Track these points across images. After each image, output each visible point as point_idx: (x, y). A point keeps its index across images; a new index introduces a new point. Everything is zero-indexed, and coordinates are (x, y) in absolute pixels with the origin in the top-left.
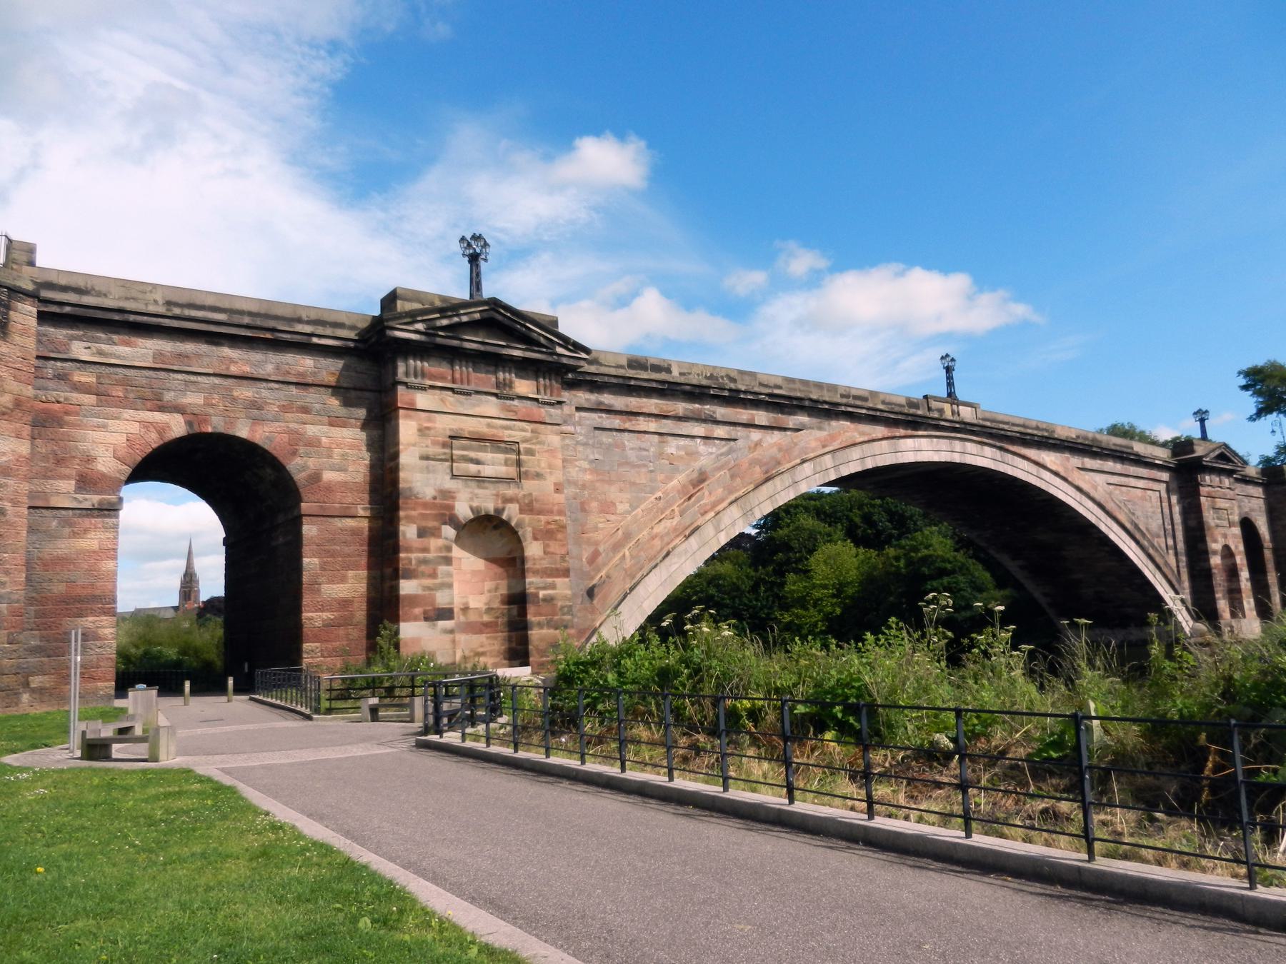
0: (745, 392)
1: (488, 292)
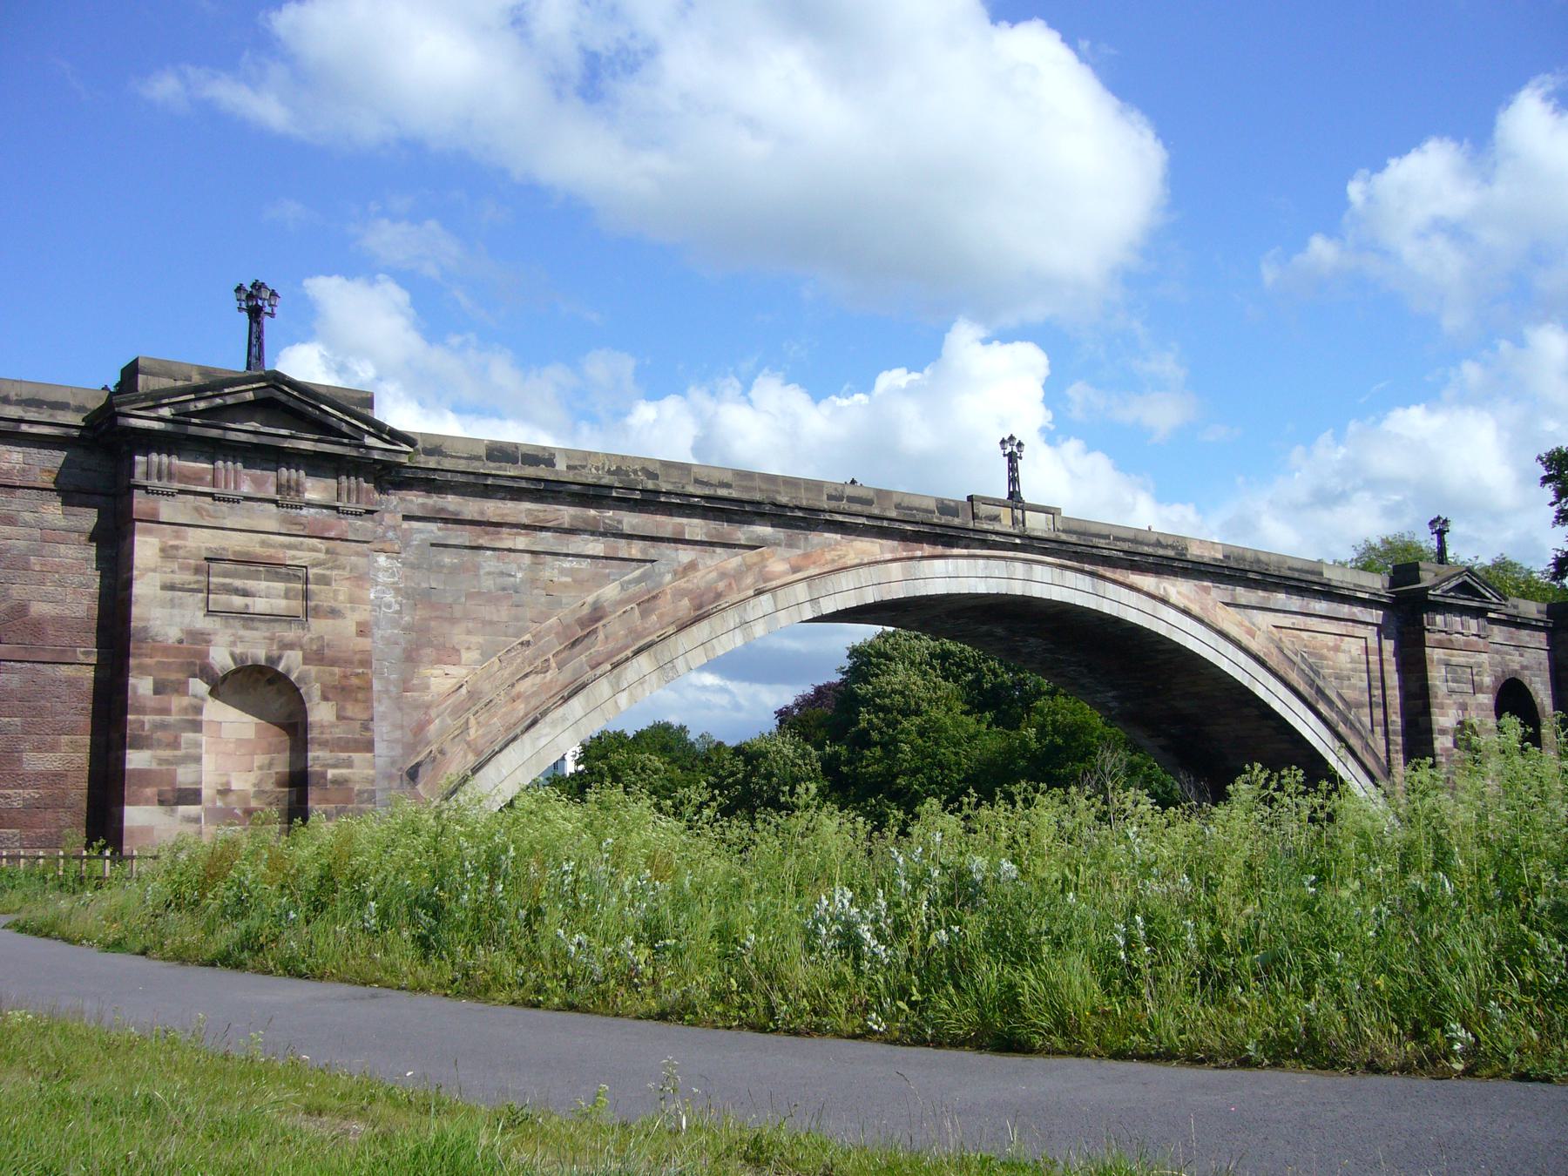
0: (668, 493)
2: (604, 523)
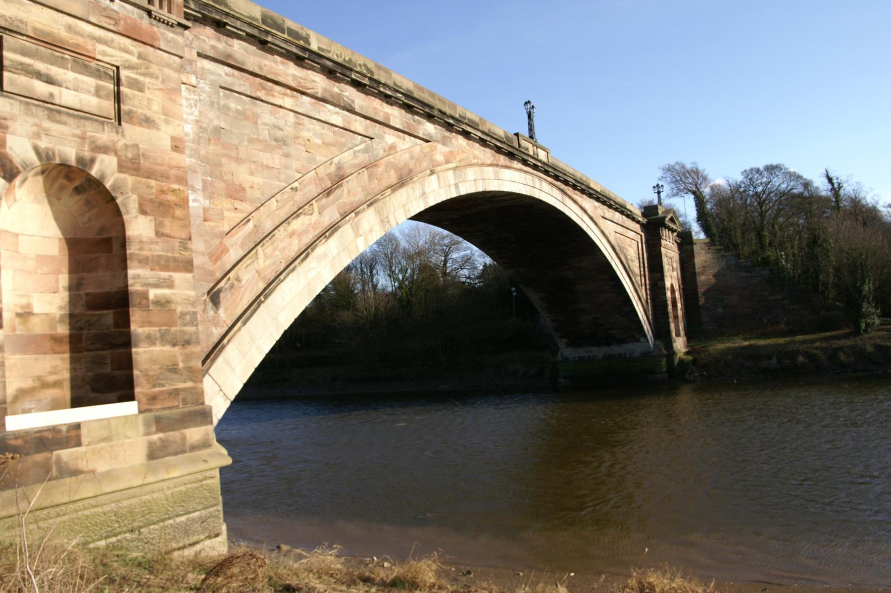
2: (344, 100)
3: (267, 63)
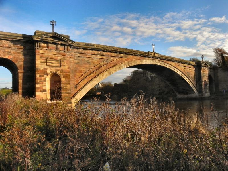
1: (55, 32)
3: (86, 51)
